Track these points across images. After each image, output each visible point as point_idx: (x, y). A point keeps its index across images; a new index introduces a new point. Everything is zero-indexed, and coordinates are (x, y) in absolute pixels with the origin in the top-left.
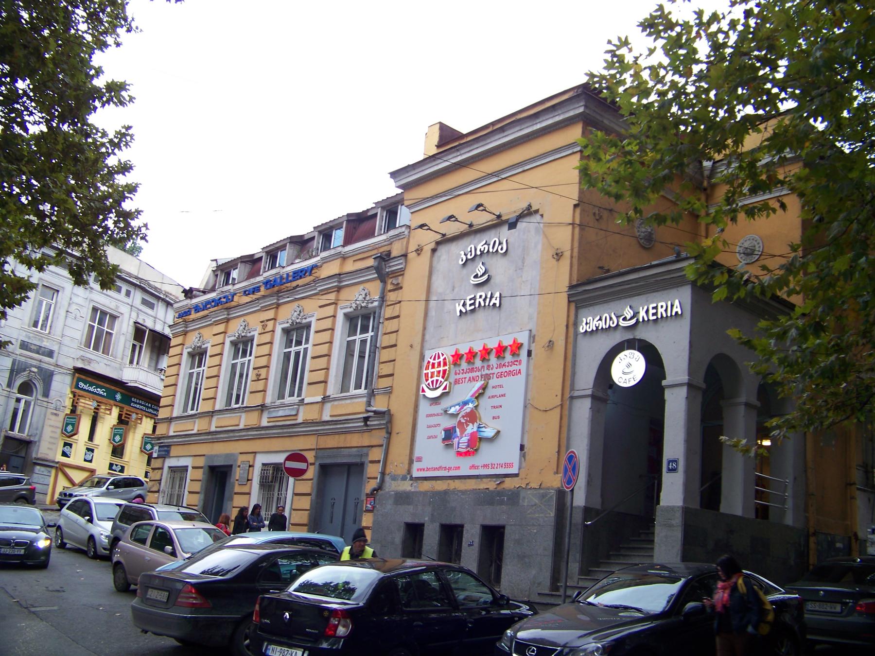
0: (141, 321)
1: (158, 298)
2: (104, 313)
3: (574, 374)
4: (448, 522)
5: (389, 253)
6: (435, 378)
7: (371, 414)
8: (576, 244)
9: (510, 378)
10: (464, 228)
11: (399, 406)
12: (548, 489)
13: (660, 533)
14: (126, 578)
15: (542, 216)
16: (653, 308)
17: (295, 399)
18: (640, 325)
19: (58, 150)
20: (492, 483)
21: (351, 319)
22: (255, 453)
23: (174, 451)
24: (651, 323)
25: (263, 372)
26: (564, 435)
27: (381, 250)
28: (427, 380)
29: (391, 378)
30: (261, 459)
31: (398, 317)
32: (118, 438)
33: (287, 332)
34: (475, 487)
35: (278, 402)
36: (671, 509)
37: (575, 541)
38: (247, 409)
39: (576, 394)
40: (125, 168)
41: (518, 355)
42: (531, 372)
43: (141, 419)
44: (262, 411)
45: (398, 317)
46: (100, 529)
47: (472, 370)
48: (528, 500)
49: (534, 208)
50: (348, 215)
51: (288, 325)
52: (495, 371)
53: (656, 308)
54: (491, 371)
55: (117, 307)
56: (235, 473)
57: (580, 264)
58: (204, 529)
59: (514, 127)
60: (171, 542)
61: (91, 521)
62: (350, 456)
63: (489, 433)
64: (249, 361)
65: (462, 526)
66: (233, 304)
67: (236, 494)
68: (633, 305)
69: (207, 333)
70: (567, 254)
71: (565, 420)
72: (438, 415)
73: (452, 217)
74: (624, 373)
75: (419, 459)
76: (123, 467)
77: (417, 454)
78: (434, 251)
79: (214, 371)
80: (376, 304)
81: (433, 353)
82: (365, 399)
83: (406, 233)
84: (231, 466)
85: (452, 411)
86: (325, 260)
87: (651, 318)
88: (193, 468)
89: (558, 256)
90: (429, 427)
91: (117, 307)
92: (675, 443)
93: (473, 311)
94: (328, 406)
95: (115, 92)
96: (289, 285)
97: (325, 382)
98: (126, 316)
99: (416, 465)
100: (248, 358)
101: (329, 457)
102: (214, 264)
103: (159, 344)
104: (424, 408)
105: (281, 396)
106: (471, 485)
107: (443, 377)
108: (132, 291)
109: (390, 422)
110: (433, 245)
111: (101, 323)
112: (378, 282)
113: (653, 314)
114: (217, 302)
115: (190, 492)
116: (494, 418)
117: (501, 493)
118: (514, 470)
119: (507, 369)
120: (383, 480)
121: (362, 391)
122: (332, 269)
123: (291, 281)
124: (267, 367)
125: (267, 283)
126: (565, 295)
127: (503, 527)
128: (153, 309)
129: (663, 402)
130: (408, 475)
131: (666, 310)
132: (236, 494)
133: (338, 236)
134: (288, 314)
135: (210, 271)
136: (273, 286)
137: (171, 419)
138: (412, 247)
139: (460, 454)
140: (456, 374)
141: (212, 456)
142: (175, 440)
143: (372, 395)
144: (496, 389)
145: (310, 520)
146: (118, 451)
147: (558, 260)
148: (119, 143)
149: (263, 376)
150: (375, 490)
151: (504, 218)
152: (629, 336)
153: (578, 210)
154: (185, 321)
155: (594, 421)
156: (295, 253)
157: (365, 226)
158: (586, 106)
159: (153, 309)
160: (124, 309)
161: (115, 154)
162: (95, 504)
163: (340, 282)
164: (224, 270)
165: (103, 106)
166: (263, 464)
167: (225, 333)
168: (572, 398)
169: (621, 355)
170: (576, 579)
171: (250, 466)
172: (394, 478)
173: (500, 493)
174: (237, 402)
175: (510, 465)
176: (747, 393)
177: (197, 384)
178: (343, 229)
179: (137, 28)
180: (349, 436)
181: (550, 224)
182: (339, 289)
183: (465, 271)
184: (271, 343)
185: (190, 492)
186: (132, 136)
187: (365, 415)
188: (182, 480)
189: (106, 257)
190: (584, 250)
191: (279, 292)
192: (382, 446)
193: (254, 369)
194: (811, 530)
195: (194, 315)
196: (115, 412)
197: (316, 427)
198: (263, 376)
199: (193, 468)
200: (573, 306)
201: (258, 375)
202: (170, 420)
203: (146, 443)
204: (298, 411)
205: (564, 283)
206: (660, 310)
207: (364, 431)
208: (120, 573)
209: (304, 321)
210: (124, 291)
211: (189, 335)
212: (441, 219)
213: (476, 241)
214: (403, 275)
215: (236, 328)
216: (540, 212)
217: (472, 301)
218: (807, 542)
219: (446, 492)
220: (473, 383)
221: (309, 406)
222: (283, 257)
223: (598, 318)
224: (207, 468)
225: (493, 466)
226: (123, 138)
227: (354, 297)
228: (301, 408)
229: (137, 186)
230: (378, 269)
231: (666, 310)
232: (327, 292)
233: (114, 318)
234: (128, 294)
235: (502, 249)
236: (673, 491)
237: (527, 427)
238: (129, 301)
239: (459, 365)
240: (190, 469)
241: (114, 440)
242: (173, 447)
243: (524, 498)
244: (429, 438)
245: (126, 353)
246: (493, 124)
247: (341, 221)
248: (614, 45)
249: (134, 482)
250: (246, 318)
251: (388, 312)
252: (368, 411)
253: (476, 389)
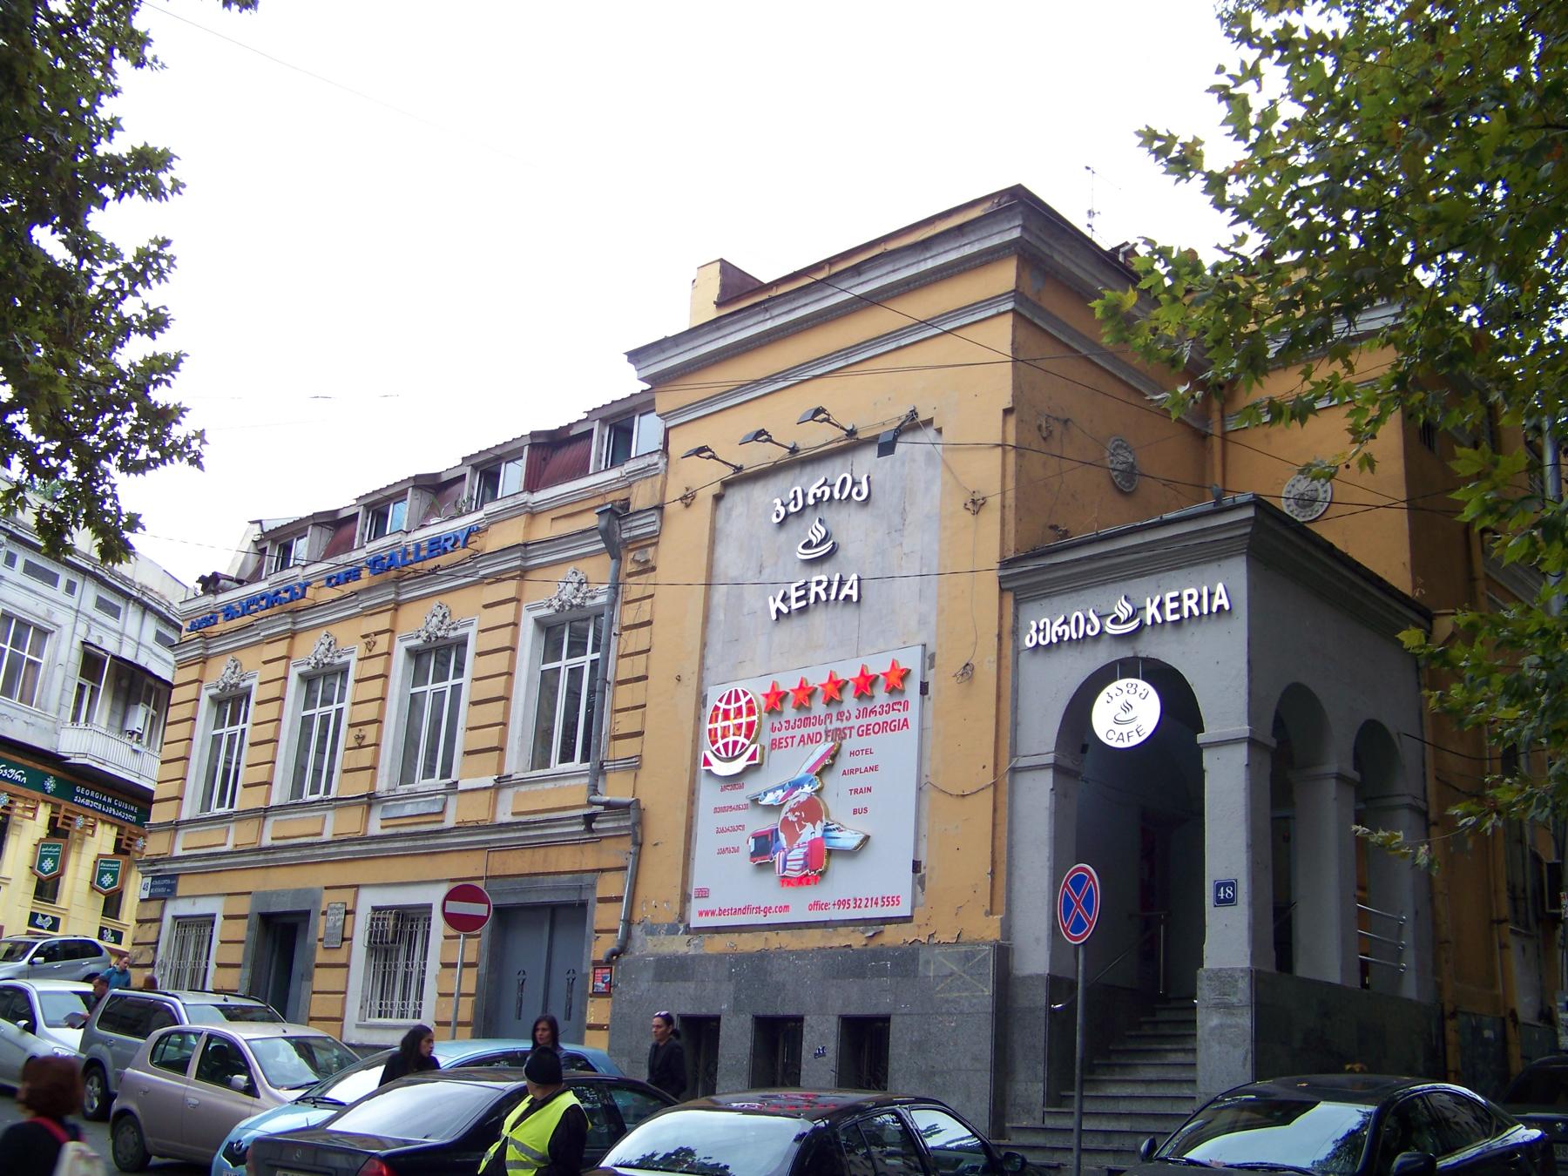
0: (94, 640)
1: (128, 597)
2: (23, 625)
3: (1015, 725)
4: (770, 1012)
5: (626, 503)
6: (731, 739)
7: (600, 809)
8: (1011, 484)
9: (888, 735)
10: (779, 454)
11: (656, 791)
12: (975, 943)
13: (1207, 1021)
14: (141, 1142)
15: (939, 431)
16: (1172, 600)
17: (437, 782)
18: (1147, 630)
19: (34, 277)
20: (858, 935)
21: (548, 629)
22: (357, 886)
23: (184, 886)
24: (1168, 626)
25: (370, 732)
26: (1003, 842)
27: (610, 498)
28: (714, 743)
29: (637, 740)
30: (368, 900)
31: (649, 623)
32: (48, 864)
33: (415, 654)
34: (821, 945)
35: (403, 789)
36: (1224, 978)
37: (1033, 1039)
38: (341, 803)
39: (1023, 762)
40: (156, 323)
41: (902, 692)
42: (929, 723)
43: (93, 827)
44: (370, 806)
45: (649, 623)
46: (53, 1044)
47: (806, 722)
48: (934, 966)
49: (922, 417)
50: (533, 435)
51: (419, 642)
52: (853, 722)
53: (1178, 599)
54: (845, 724)
55: (50, 613)
56: (316, 926)
57: (1019, 520)
58: (287, 1039)
59: (881, 265)
60: (246, 1068)
61: (32, 1028)
62: (555, 889)
63: (848, 839)
64: (243, 731)
65: (799, 1020)
66: (303, 603)
67: (318, 966)
68: (1131, 596)
69: (249, 659)
70: (995, 501)
71: (1003, 812)
72: (738, 808)
73: (761, 433)
74: (1117, 722)
75: (703, 893)
76: (56, 922)
77: (697, 882)
78: (718, 498)
79: (267, 732)
80: (602, 599)
81: (725, 690)
82: (586, 781)
83: (661, 465)
84: (308, 913)
85: (770, 799)
86: (494, 519)
87: (1170, 618)
88: (226, 917)
89: (976, 505)
90: (720, 831)
91: (50, 613)
92: (1227, 844)
93: (802, 610)
94: (507, 795)
95: (144, 171)
96: (418, 566)
97: (500, 749)
98: (67, 630)
99: (696, 905)
100: (241, 726)
101: (514, 892)
102: (256, 529)
103: (132, 685)
104: (709, 795)
105: (406, 776)
106: (813, 939)
107: (747, 737)
108: (79, 582)
109: (639, 823)
110: (716, 488)
111: (18, 642)
112: (607, 557)
113: (1173, 611)
114: (272, 600)
115: (219, 965)
116: (855, 812)
117: (877, 953)
118: (903, 910)
119: (885, 718)
120: (628, 935)
121: (576, 765)
122: (510, 534)
123: (425, 559)
124: (378, 721)
125: (376, 564)
126: (993, 578)
127: (886, 1019)
128: (117, 617)
129: (1201, 773)
130: (680, 925)
131: (1199, 603)
132: (318, 966)
133: (513, 476)
134: (419, 621)
135: (247, 545)
136: (389, 569)
137: (178, 823)
138: (674, 492)
139: (786, 881)
140: (773, 729)
141: (265, 893)
142: (187, 865)
143: (600, 771)
144: (857, 758)
145: (476, 1013)
146: (47, 889)
147: (976, 513)
148: (144, 272)
149: (370, 740)
150: (613, 953)
151: (861, 436)
152: (1125, 652)
153: (1012, 420)
154: (203, 636)
155: (1058, 814)
156: (424, 507)
157: (566, 455)
158: (1024, 228)
159: (117, 617)
160: (63, 618)
161: (136, 294)
162: (40, 994)
163: (525, 559)
164: (277, 542)
165: (119, 196)
166: (375, 909)
167: (288, 657)
168: (1014, 770)
169: (1111, 688)
170: (1038, 1114)
171: (347, 913)
172: (652, 930)
173: (879, 954)
174: (315, 791)
175: (895, 900)
176: (1337, 757)
177: (228, 762)
178: (523, 463)
179: (155, 60)
180: (553, 852)
181: (956, 446)
182: (523, 574)
183: (783, 536)
184: (385, 676)
185: (219, 965)
186: (171, 260)
187: (587, 811)
188: (204, 942)
189: (115, 497)
190: (1027, 494)
191: (399, 579)
192: (625, 868)
193: (351, 726)
194: (1449, 1008)
195: (222, 626)
196: (44, 813)
197: (484, 835)
198: (370, 740)
199: (226, 917)
200: (1009, 599)
201: (360, 738)
202: (175, 826)
203: (102, 873)
204: (445, 805)
205: (990, 554)
206: (1186, 603)
207: (586, 842)
208: (128, 1135)
209: (452, 634)
210: (62, 583)
211: (211, 662)
212: (740, 439)
213: (804, 479)
214: (656, 544)
215: (310, 649)
216: (936, 424)
217: (802, 592)
218: (1442, 1028)
219: (763, 955)
220: (810, 746)
221: (468, 796)
222: (399, 514)
223: (1061, 619)
224: (256, 919)
225: (857, 903)
226: (150, 264)
227: (550, 592)
228: (452, 800)
229: (178, 359)
230: (607, 534)
231: (1199, 603)
232: (497, 578)
233: (43, 633)
234: (71, 588)
235: (859, 494)
236: (1227, 940)
237: (925, 829)
238: (72, 601)
239: (780, 713)
240: (219, 920)
241: (41, 868)
242: (181, 879)
243: (927, 962)
244: (722, 851)
245: (65, 702)
246: (830, 262)
247: (517, 445)
248: (1231, 77)
249: (83, 949)
250: (331, 629)
251: (629, 615)
252: (591, 803)
253: (817, 756)
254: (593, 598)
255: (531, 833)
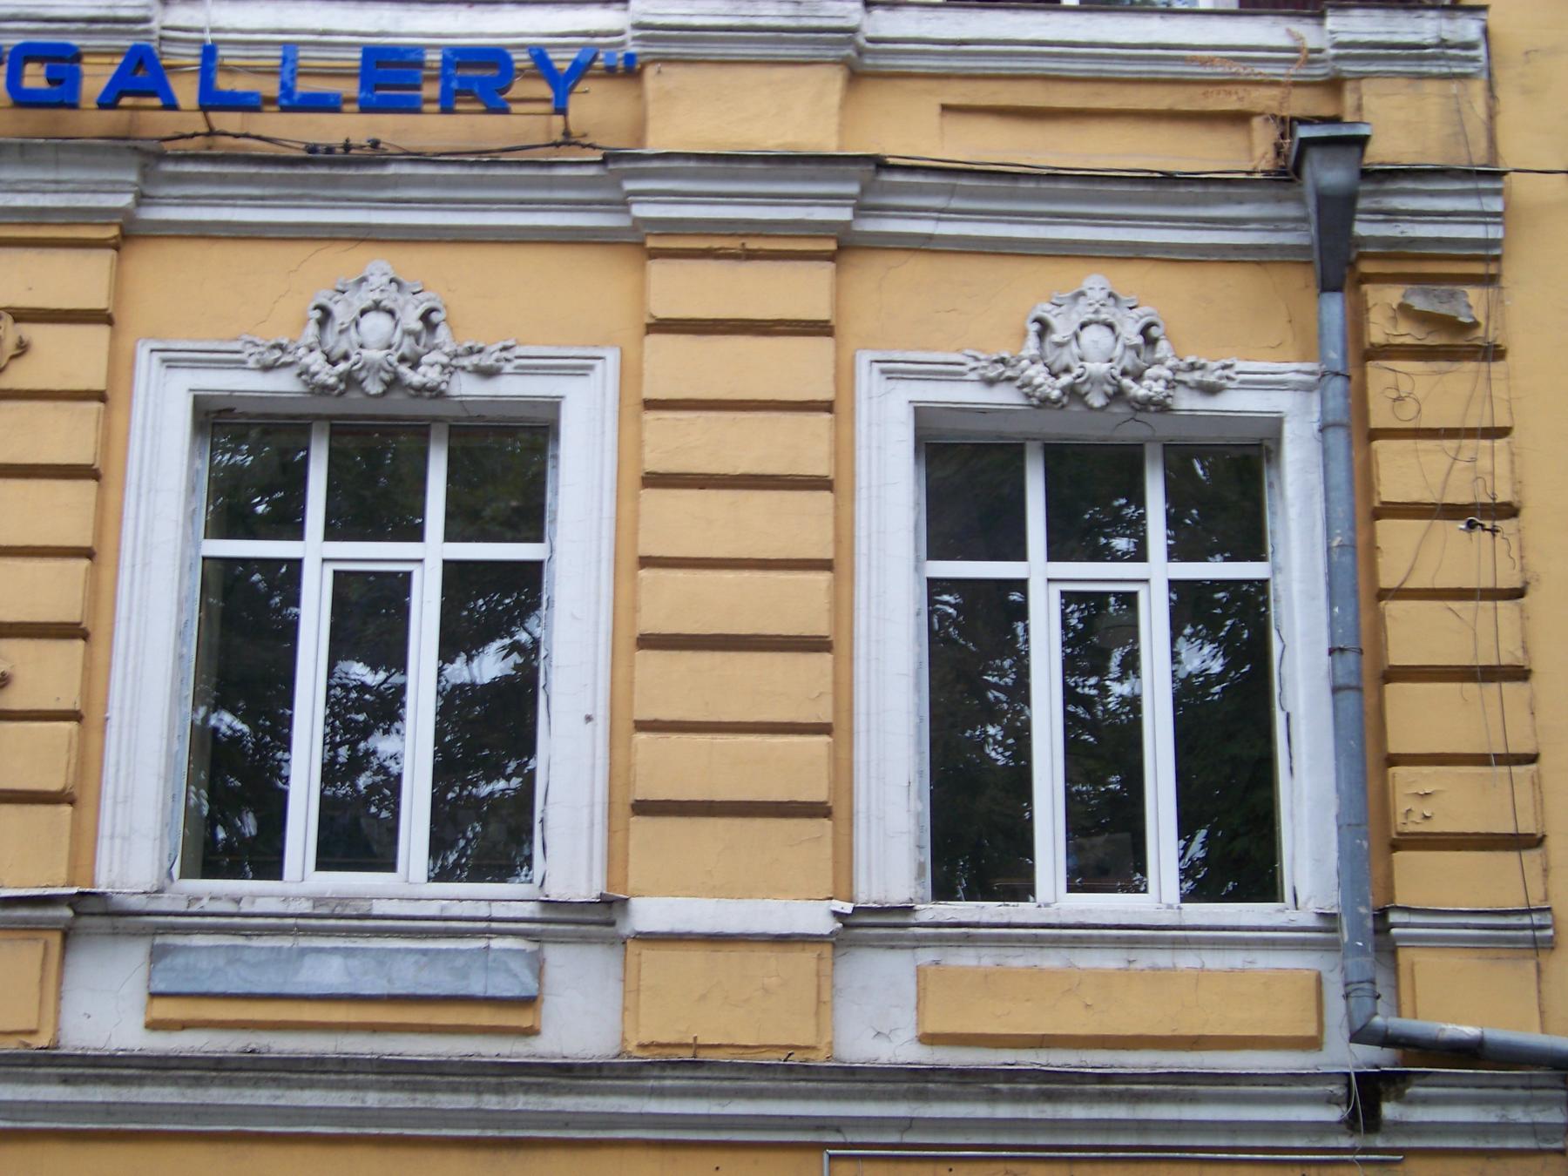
254: (1211, 390)
255: (1078, 1112)
